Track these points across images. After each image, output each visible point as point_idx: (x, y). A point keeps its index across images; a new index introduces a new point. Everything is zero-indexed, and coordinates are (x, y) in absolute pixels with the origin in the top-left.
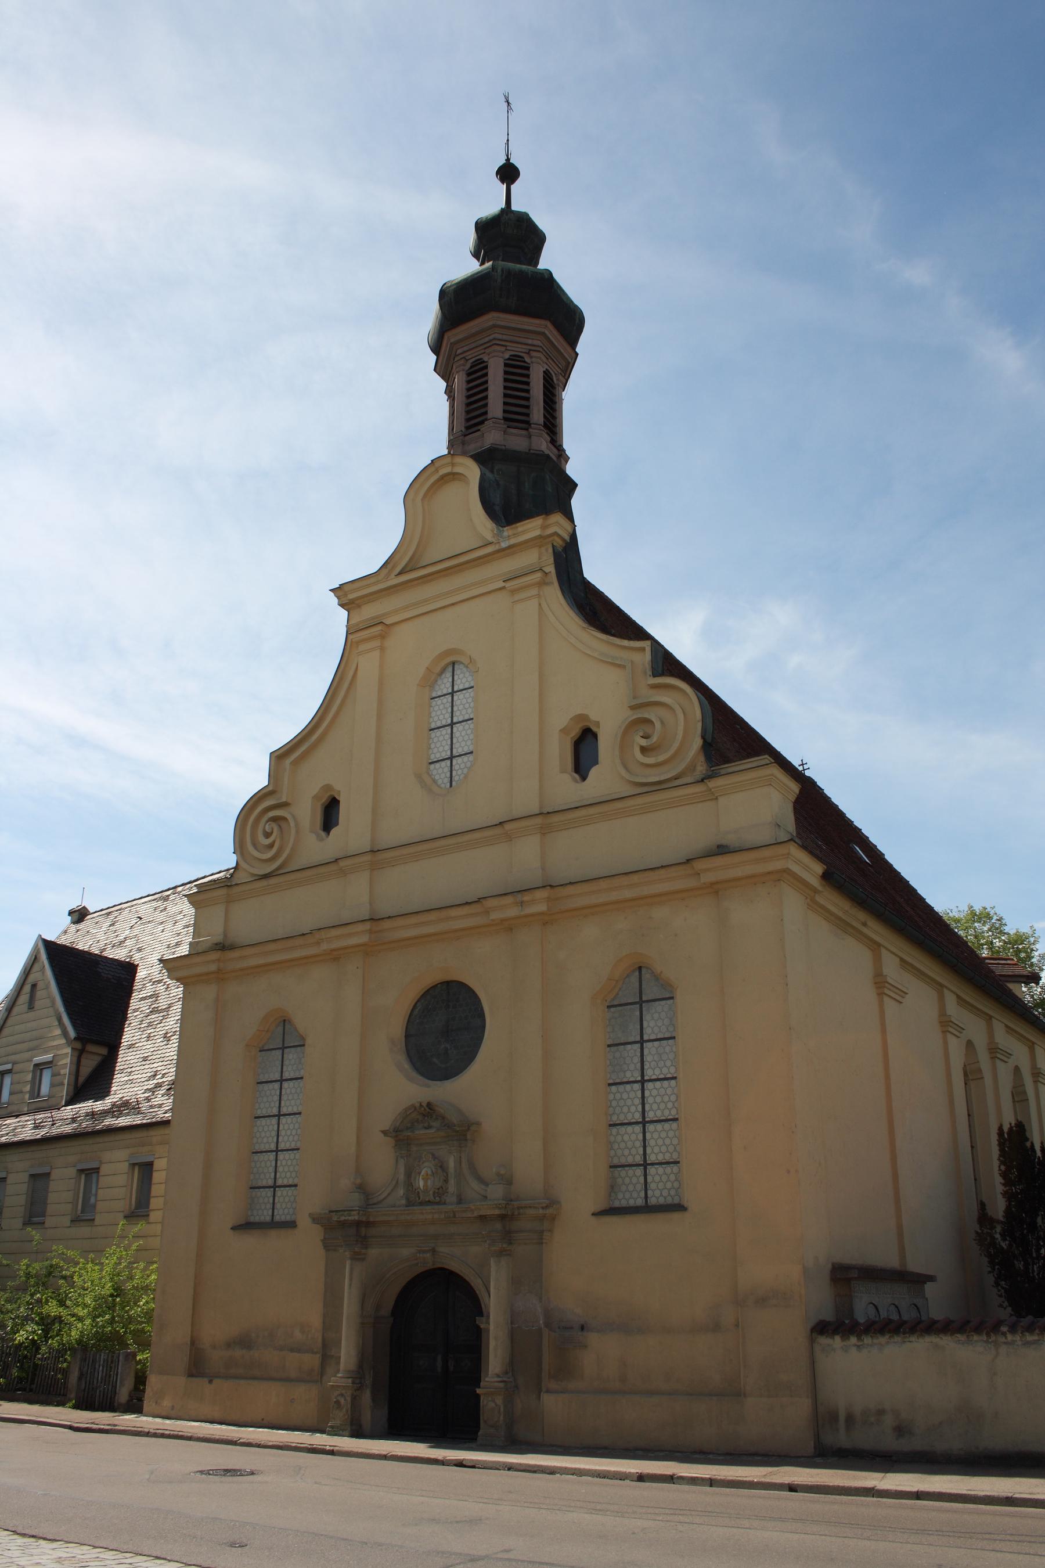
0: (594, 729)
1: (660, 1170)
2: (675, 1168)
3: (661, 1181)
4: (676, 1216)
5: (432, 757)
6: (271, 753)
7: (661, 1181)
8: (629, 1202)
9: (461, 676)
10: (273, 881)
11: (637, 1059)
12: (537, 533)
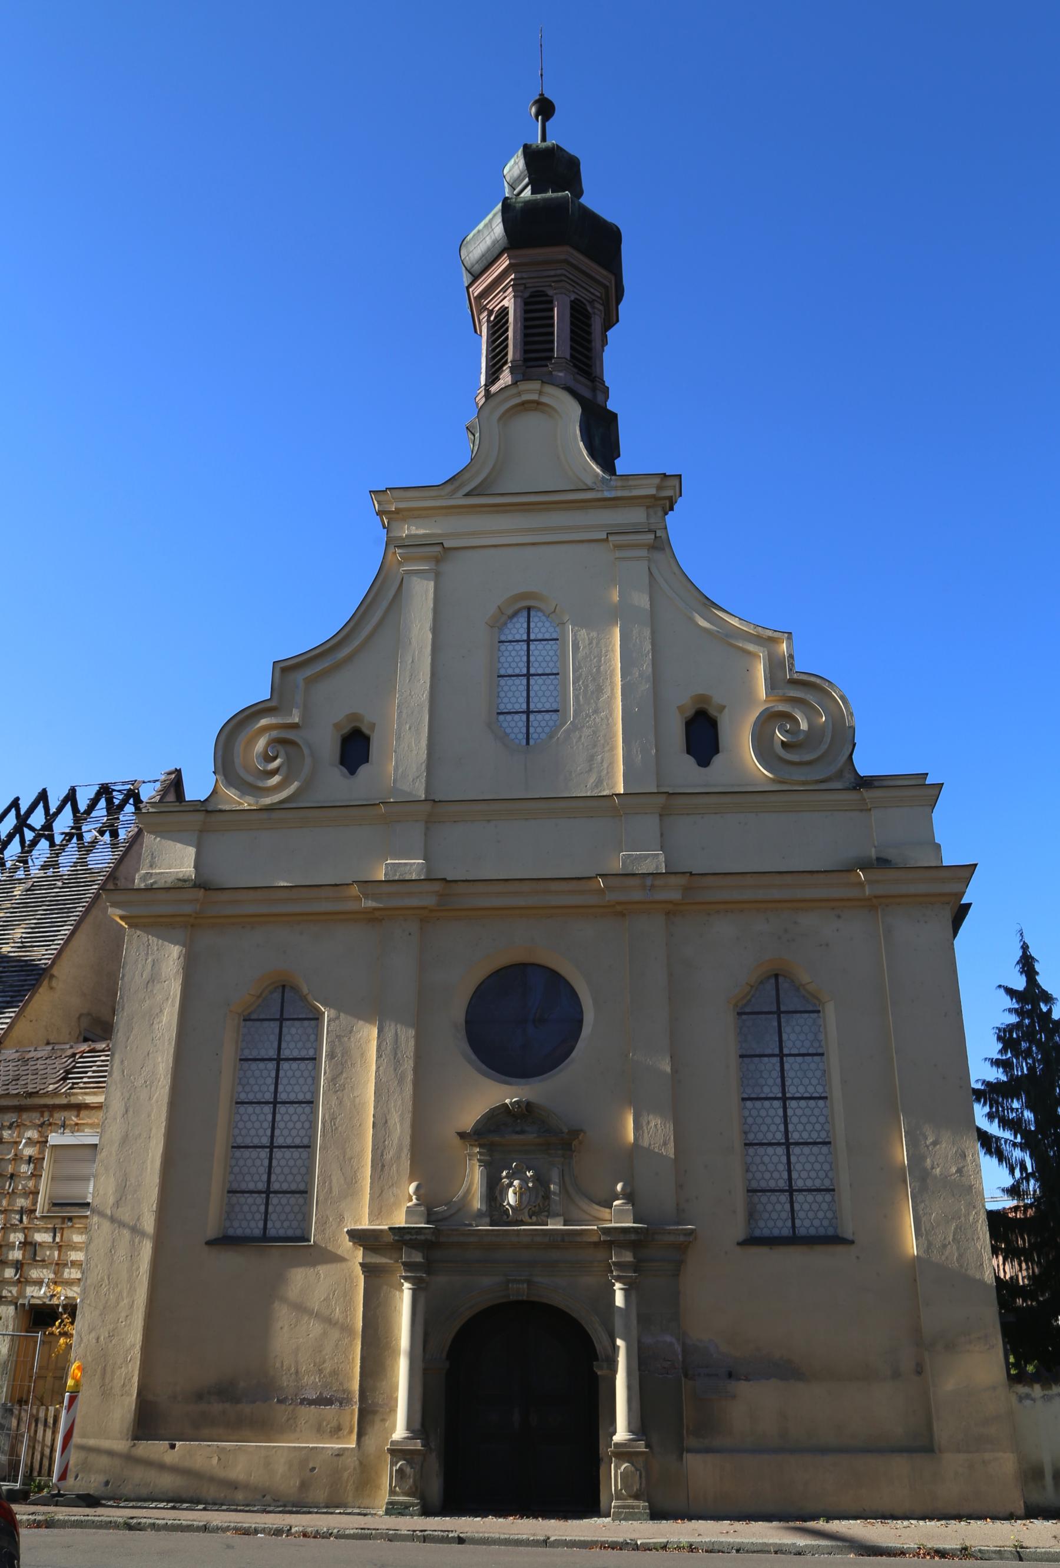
0: (713, 712)
1: (810, 1197)
2: (828, 1197)
3: (811, 1209)
4: (840, 1249)
5: (502, 706)
6: (274, 662)
7: (811, 1209)
8: (809, 1231)
9: (540, 624)
10: (276, 815)
11: (776, 1074)
12: (653, 491)
